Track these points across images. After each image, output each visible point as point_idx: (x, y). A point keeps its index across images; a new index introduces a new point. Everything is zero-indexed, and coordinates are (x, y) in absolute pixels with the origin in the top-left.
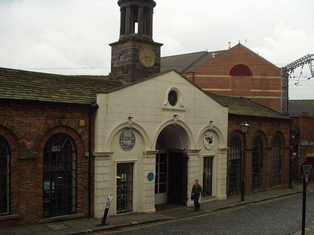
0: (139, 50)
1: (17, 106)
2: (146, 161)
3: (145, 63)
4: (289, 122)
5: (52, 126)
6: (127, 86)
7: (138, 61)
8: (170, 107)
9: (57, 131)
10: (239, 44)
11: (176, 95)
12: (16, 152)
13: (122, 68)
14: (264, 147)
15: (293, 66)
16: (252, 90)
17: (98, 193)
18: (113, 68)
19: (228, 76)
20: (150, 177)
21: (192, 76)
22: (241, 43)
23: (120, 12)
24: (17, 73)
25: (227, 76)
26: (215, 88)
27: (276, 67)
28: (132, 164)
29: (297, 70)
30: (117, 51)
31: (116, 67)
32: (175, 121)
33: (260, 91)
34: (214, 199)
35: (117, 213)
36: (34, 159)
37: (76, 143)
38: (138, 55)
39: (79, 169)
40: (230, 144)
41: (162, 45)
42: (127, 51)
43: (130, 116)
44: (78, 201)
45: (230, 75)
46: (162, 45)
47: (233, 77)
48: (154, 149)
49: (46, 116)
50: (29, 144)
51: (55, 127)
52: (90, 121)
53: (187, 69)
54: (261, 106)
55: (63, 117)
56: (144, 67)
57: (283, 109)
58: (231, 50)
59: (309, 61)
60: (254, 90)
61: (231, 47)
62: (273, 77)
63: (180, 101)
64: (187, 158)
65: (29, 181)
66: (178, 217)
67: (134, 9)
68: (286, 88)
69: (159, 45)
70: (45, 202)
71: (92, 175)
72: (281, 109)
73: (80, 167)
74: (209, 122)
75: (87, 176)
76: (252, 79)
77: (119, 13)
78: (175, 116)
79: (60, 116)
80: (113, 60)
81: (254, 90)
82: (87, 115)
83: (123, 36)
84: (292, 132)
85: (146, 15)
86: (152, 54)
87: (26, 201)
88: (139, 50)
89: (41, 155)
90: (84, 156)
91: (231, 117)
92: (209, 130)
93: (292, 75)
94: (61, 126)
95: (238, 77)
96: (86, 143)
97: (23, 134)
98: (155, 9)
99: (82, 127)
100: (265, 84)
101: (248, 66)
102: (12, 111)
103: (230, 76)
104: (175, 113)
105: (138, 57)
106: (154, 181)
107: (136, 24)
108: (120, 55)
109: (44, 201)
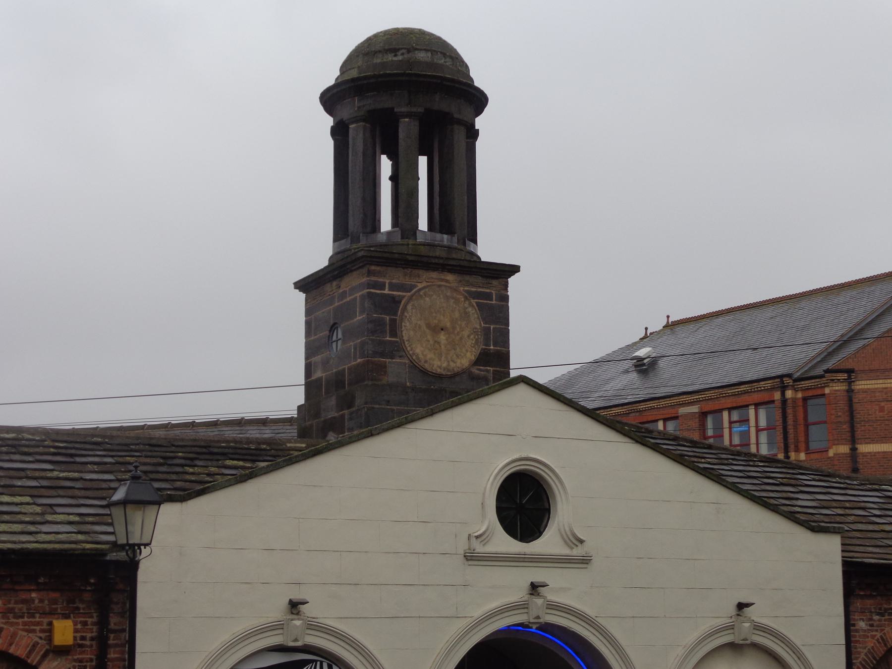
3: (430, 355)
7: (397, 349)
11: (538, 482)
18: (312, 387)
21: (842, 387)
23: (331, 142)
31: (320, 379)
38: (393, 322)
41: (514, 269)
52: (103, 623)
56: (424, 372)
74: (733, 610)
78: (534, 588)
80: (311, 350)
82: (87, 596)
86: (465, 315)
88: (395, 302)
92: (733, 647)
105: (394, 333)
108: (333, 328)
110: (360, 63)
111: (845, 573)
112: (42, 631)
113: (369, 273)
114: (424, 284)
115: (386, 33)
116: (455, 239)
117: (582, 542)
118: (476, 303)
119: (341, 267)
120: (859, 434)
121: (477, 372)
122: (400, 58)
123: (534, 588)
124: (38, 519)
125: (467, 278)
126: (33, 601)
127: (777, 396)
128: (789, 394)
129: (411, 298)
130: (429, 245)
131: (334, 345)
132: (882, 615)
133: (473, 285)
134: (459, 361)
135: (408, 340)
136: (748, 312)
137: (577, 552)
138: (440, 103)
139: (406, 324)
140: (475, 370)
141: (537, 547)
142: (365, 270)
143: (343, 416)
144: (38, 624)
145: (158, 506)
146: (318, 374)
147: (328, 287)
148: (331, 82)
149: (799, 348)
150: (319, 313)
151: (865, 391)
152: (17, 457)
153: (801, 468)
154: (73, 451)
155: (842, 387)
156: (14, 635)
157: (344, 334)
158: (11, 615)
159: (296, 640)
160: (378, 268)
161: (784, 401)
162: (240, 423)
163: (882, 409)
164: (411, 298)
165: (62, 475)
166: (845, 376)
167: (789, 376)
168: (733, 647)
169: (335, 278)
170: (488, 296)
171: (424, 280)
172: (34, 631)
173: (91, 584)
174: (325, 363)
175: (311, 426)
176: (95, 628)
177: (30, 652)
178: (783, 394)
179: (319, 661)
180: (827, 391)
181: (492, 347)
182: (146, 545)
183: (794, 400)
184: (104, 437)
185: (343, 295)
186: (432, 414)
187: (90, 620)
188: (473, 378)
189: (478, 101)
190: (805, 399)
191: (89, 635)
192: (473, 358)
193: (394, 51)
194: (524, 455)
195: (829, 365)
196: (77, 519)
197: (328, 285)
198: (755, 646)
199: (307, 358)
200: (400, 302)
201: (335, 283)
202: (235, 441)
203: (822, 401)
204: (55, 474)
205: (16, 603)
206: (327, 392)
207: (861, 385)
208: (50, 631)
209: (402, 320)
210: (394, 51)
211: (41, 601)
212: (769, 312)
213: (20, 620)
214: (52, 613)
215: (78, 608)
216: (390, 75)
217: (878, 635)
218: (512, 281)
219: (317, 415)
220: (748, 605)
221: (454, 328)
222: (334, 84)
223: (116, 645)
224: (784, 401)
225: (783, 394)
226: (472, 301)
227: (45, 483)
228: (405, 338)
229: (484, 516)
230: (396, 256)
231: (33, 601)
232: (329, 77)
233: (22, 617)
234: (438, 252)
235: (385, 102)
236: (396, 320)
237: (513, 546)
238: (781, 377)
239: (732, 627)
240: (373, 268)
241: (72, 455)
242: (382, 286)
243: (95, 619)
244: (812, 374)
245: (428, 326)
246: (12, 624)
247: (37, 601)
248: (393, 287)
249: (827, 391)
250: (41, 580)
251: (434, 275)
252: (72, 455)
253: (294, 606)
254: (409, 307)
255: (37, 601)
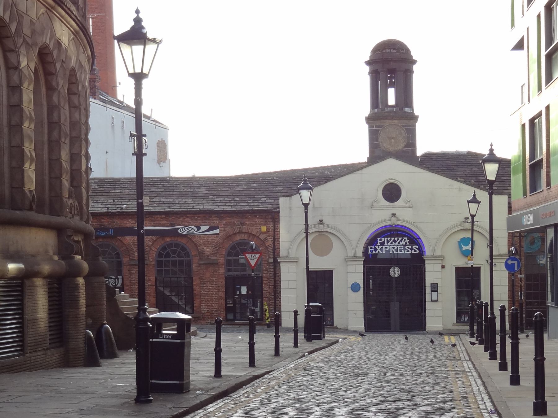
1: (194, 217)
2: (350, 269)
9: (239, 238)
16: (484, 338)
17: (284, 300)
20: (355, 287)
55: (242, 224)
65: (209, 284)
66: (278, 375)
75: (272, 282)
94: (241, 232)
96: (270, 249)
99: (264, 233)
101: (506, 269)
102: (190, 221)
106: (361, 291)
112: (259, 228)
118: (405, 129)
121: (405, 150)
126: (521, 274)
129: (382, 129)
134: (398, 147)
135: (381, 143)
140: (404, 149)
144: (258, 227)
158: (252, 225)
170: (409, 126)
172: (257, 228)
177: (257, 233)
179: (414, 249)
181: (410, 142)
200: (379, 131)
205: (253, 222)
211: (259, 221)
214: (261, 224)
226: (403, 128)
228: (380, 142)
231: (256, 221)
233: (254, 225)
236: (377, 137)
237: (387, 203)
247: (257, 221)
250: (258, 217)
254: (381, 132)
255: (257, 221)
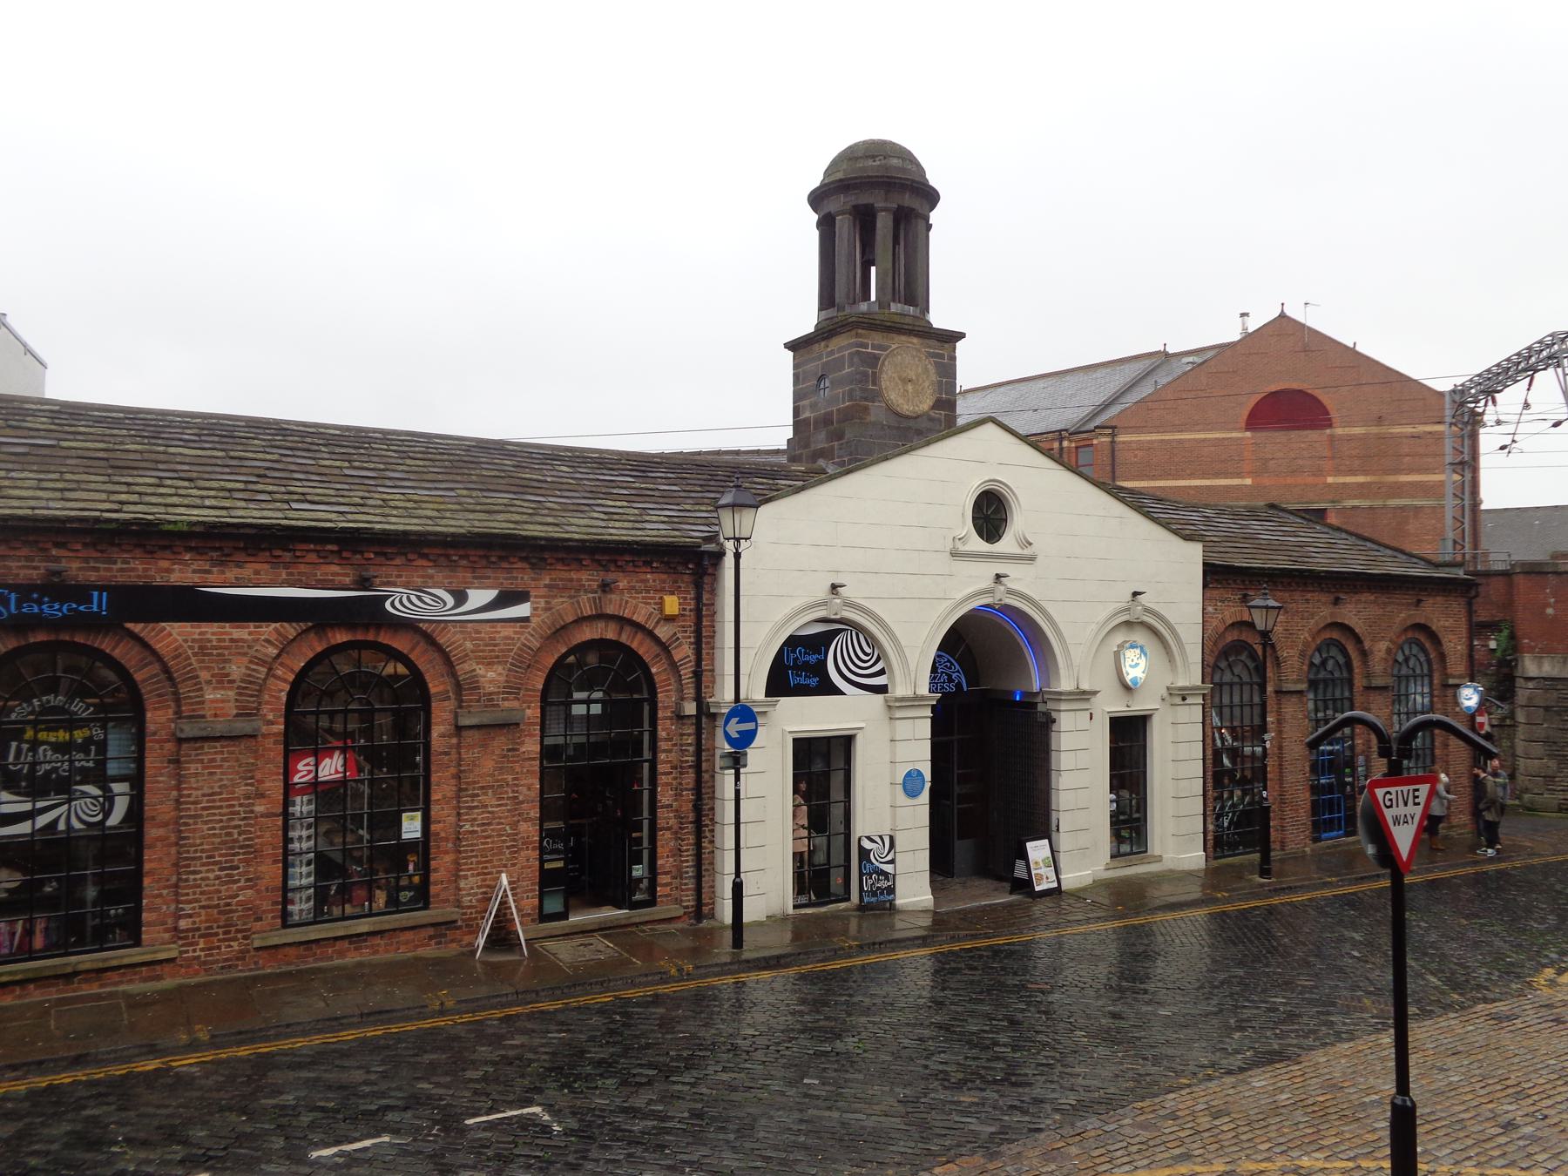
0: (876, 358)
3: (901, 401)
4: (1464, 588)
5: (571, 619)
6: (832, 478)
7: (876, 395)
8: (978, 544)
9: (588, 633)
10: (1282, 316)
11: (1000, 501)
12: (446, 703)
13: (826, 420)
14: (1359, 682)
15: (1492, 383)
16: (1330, 480)
18: (797, 425)
19: (1240, 435)
20: (910, 785)
21: (1108, 439)
22: (1288, 313)
24: (468, 449)
25: (1234, 435)
26: (1192, 476)
27: (1429, 389)
28: (846, 743)
29: (1511, 397)
30: (810, 367)
31: (808, 419)
32: (1001, 597)
33: (1361, 479)
34: (1153, 868)
35: (795, 907)
36: (509, 726)
37: (654, 670)
38: (874, 374)
39: (662, 756)
40: (1210, 669)
41: (961, 336)
42: (838, 364)
43: (837, 582)
44: (660, 862)
45: (1247, 429)
46: (961, 336)
47: (1259, 434)
48: (924, 690)
49: (546, 586)
50: (491, 677)
51: (581, 620)
52: (698, 598)
53: (1095, 415)
54: (1347, 532)
55: (605, 587)
56: (897, 414)
57: (1455, 542)
58: (1249, 338)
59: (1554, 360)
60: (1341, 480)
61: (1250, 330)
62: (1409, 430)
63: (1019, 523)
64: (1049, 721)
65: (489, 798)
67: (865, 219)
68: (1469, 464)
69: (952, 338)
70: (547, 866)
71: (706, 776)
72: (1450, 544)
73: (665, 751)
74: (1129, 597)
75: (689, 779)
76: (1332, 438)
77: (814, 236)
79: (595, 585)
80: (797, 397)
81: (1341, 480)
83: (832, 312)
84: (1478, 629)
85: (902, 227)
86: (926, 370)
87: (478, 863)
88: (876, 358)
89: (533, 712)
90: (680, 717)
91: (1214, 575)
92: (1128, 624)
93: (1489, 418)
95: (1280, 436)
96: (686, 672)
97: (469, 645)
98: (934, 217)
99: (670, 619)
100: (1378, 454)
101: (1319, 394)
102: (430, 571)
103: (1248, 434)
104: (1001, 568)
105: (874, 384)
106: (925, 796)
107: (873, 269)
108: (821, 378)
109: (542, 862)
110: (845, 166)
111: (1205, 573)
112: (656, 604)
113: (857, 335)
114: (897, 345)
115: (865, 142)
116: (918, 311)
117: (1030, 544)
119: (830, 330)
120: (1117, 474)
122: (878, 163)
123: (998, 577)
124: (639, 519)
125: (927, 341)
127: (1056, 445)
128: (1065, 444)
129: (887, 356)
130: (901, 314)
131: (822, 392)
132: (1223, 602)
133: (930, 347)
136: (1023, 384)
137: (1027, 552)
138: (908, 200)
139: (884, 376)
140: (932, 413)
141: (999, 547)
142: (854, 332)
143: (833, 447)
145: (754, 510)
146: (806, 414)
147: (816, 347)
148: (817, 184)
149: (1070, 411)
150: (808, 367)
151: (1124, 443)
152: (605, 471)
153: (1141, 494)
154: (643, 468)
155: (1108, 439)
156: (636, 607)
157: (832, 383)
159: (836, 614)
160: (863, 332)
161: (1061, 449)
162: (718, 453)
163: (1136, 456)
164: (887, 356)
165: (643, 486)
166: (1110, 431)
167: (1066, 430)
168: (1128, 624)
169: (824, 339)
170: (941, 356)
171: (897, 342)
172: (650, 604)
173: (689, 569)
174: (813, 406)
175: (802, 454)
176: (692, 602)
178: (1061, 444)
180: (1095, 442)
182: (746, 539)
183: (1069, 448)
184: (661, 458)
185: (832, 352)
186: (928, 444)
187: (689, 596)
188: (931, 419)
189: (932, 197)
190: (1077, 448)
191: (688, 608)
192: (931, 404)
193: (873, 157)
194: (987, 479)
195: (1098, 422)
196: (666, 519)
197: (817, 345)
198: (1143, 624)
199: (794, 403)
201: (823, 344)
202: (755, 464)
203: (1091, 449)
204: (637, 485)
205: (637, 582)
206: (815, 429)
207: (1121, 438)
208: (661, 603)
209: (881, 373)
210: (873, 157)
211: (654, 581)
212: (1041, 384)
213: (640, 595)
214: (662, 590)
215: (680, 587)
216: (871, 177)
217: (1220, 616)
218: (959, 345)
219: (807, 446)
220: (1140, 593)
221: (918, 380)
222: (823, 185)
223: (708, 616)
224: (1061, 449)
225: (1061, 444)
227: (633, 492)
229: (964, 523)
230: (878, 322)
232: (815, 180)
234: (907, 320)
235: (864, 199)
238: (1060, 431)
239: (1128, 610)
240: (860, 331)
241: (644, 471)
242: (865, 346)
243: (692, 596)
244: (1082, 429)
245: (900, 378)
246: (635, 598)
248: (874, 347)
249: (1095, 442)
250: (655, 565)
251: (903, 338)
252: (644, 471)
253: (834, 588)
254: (886, 363)
